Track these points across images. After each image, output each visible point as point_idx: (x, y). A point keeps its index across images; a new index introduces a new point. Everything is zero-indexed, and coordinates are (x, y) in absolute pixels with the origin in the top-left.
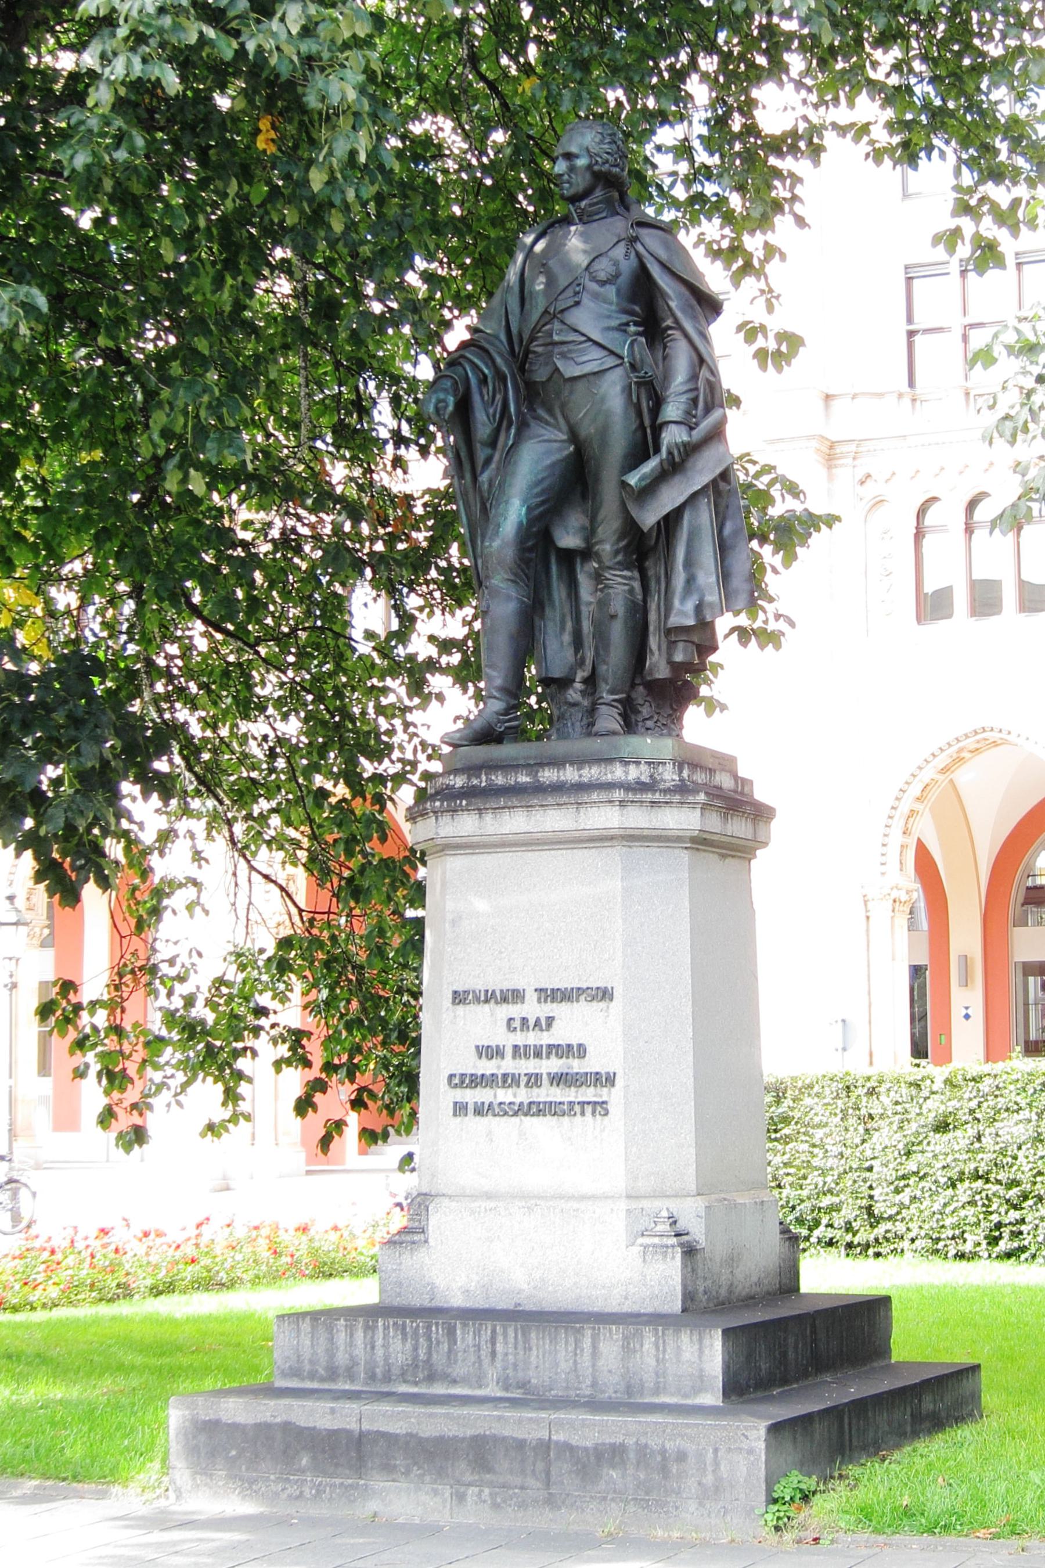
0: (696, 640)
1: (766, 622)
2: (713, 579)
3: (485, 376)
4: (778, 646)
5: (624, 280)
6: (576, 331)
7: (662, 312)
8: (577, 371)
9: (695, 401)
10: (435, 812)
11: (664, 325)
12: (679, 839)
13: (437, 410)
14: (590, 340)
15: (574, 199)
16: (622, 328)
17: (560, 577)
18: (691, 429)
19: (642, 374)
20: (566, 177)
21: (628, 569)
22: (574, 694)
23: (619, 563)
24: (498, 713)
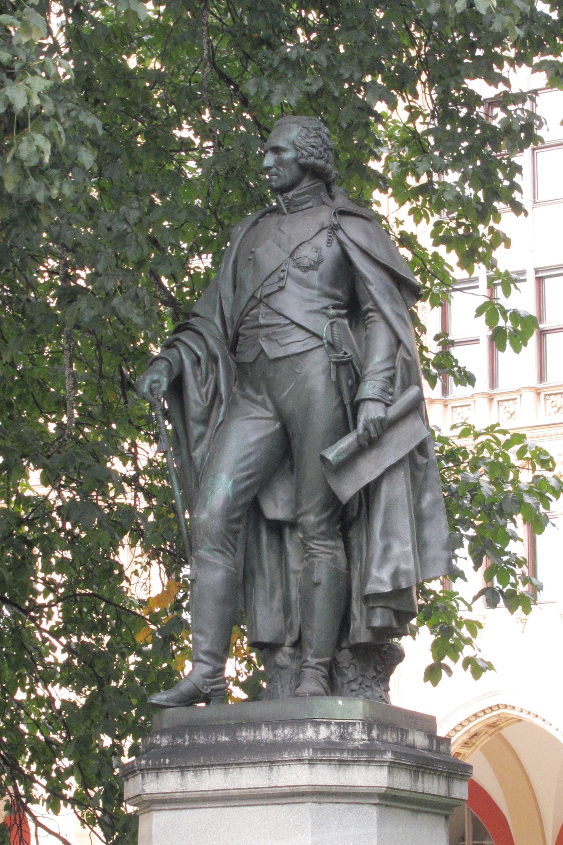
0: (393, 605)
1: (514, 585)
2: (409, 548)
3: (199, 359)
4: (527, 610)
5: (326, 267)
6: (280, 314)
7: (362, 297)
8: (280, 353)
9: (392, 380)
10: (141, 770)
11: (365, 308)
12: (367, 795)
13: (151, 390)
14: (293, 322)
15: (282, 190)
16: (322, 311)
17: (270, 546)
18: (387, 405)
19: (341, 354)
20: (274, 170)
21: (331, 538)
22: (283, 658)
23: (322, 533)
24: (205, 676)
